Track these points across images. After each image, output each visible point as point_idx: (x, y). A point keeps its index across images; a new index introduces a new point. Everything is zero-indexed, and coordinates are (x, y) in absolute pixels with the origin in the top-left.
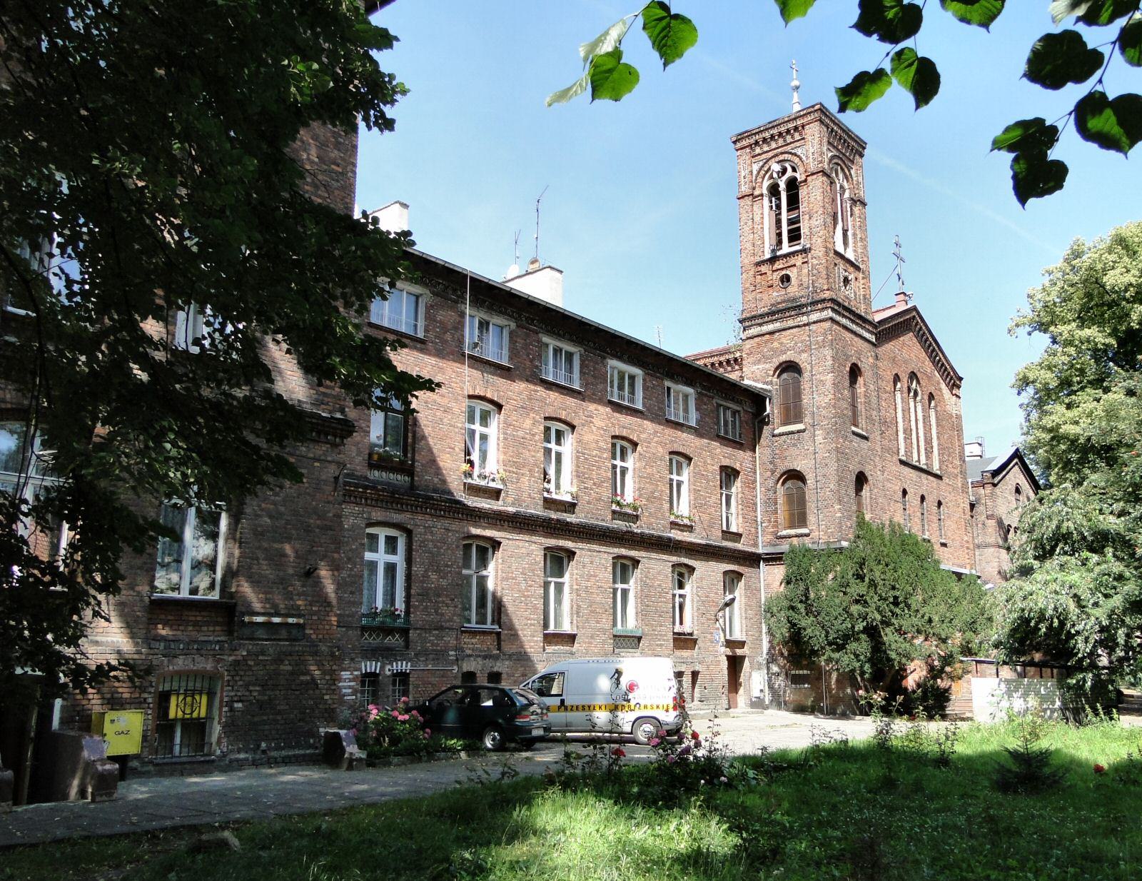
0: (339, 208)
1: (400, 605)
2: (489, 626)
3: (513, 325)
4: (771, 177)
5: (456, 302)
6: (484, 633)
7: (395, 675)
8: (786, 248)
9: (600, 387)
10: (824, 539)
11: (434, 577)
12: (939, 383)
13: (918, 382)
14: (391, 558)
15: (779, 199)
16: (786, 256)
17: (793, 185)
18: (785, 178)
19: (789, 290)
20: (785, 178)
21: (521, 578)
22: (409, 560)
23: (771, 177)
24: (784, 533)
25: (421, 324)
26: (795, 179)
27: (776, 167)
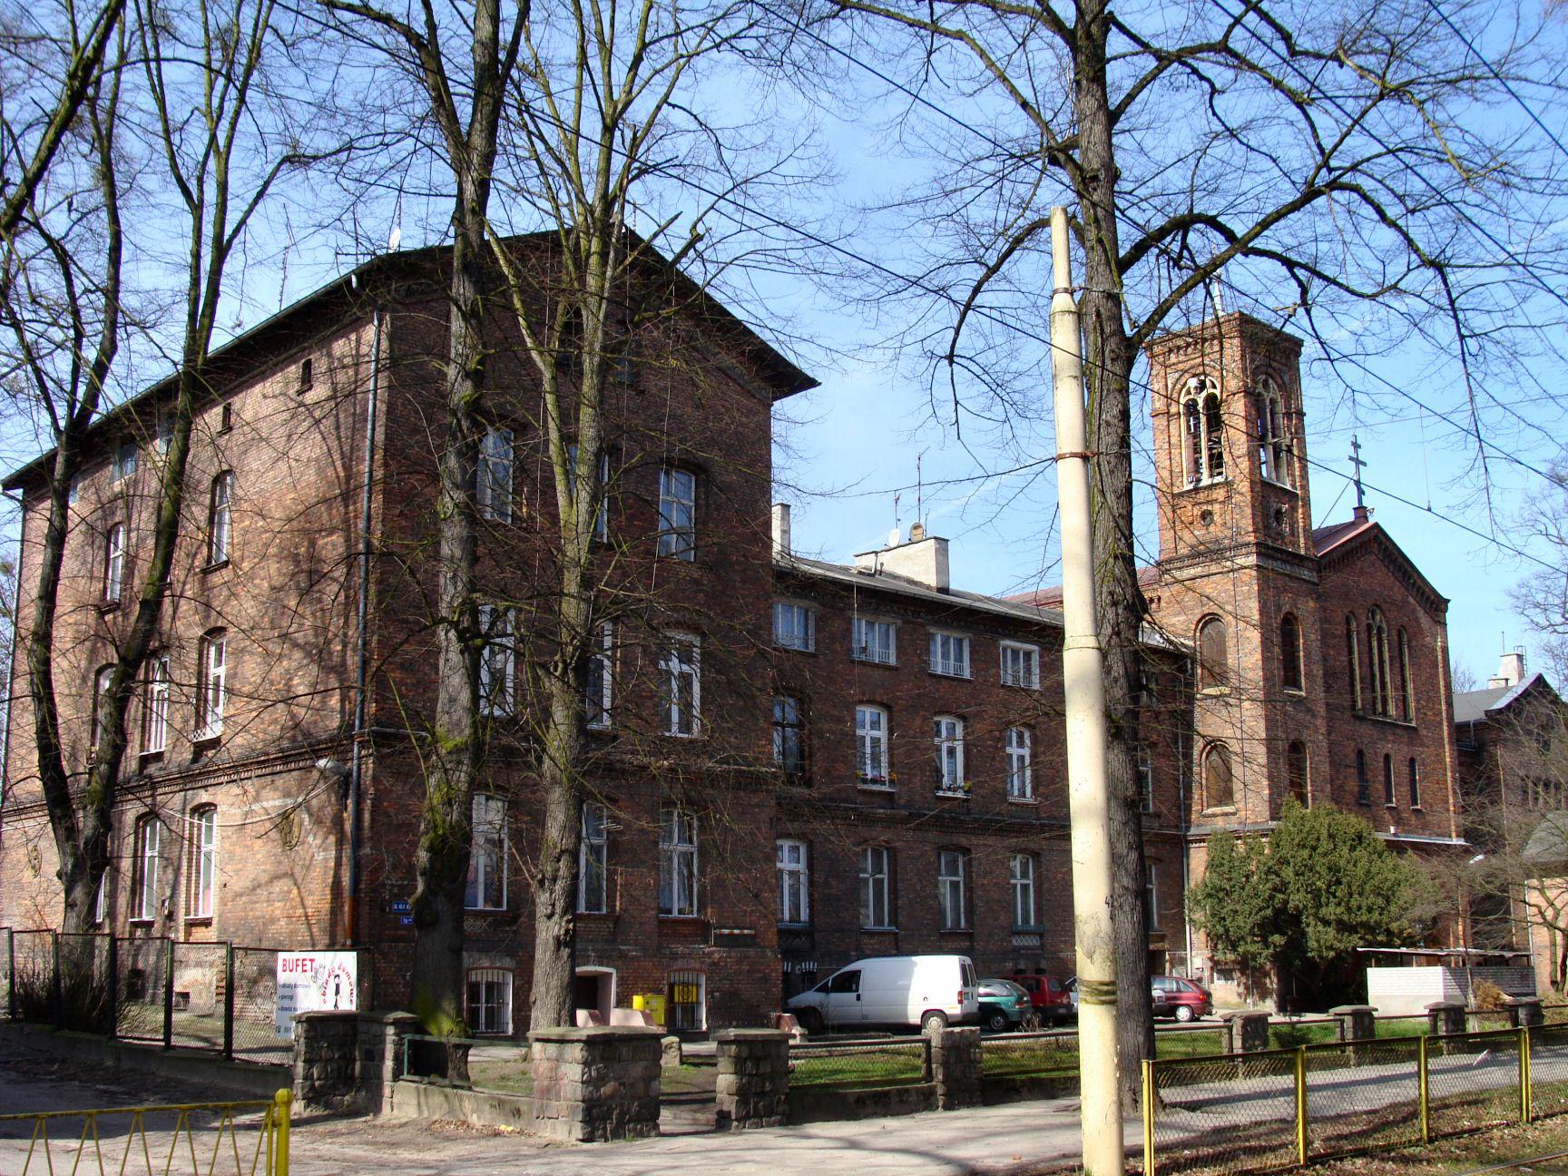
0: (902, 1021)
1: (804, 914)
2: (886, 927)
3: (899, 622)
4: (1189, 392)
5: (843, 610)
6: (883, 933)
7: (804, 974)
8: (1206, 481)
9: (993, 671)
10: (1252, 818)
11: (834, 882)
12: (1414, 611)
13: (1383, 612)
14: (1021, 751)
15: (1197, 419)
16: (1205, 488)
17: (1212, 402)
18: (1204, 394)
19: (1212, 528)
20: (1204, 394)
21: (915, 880)
22: (810, 866)
23: (1189, 392)
24: (1210, 811)
25: (811, 643)
26: (1214, 396)
27: (1193, 383)
